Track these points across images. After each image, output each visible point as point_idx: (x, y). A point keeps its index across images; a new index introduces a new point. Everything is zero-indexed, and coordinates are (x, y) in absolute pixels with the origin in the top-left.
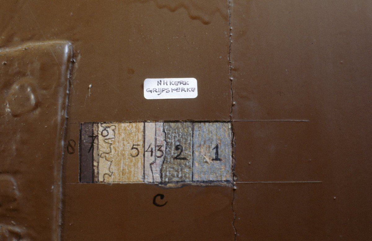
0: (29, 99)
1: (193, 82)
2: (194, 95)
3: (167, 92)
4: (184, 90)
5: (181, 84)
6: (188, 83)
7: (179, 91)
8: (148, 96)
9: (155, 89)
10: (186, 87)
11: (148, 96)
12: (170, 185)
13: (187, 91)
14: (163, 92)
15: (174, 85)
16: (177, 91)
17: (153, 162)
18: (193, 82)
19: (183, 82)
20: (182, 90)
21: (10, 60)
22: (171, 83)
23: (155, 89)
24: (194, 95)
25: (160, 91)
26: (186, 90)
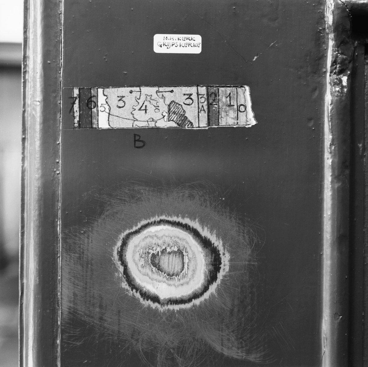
0: (158, 298)
1: (198, 39)
2: (198, 50)
3: (176, 46)
4: (188, 39)
5: (188, 40)
6: (194, 39)
7: (186, 47)
8: (157, 49)
9: (166, 44)
10: (192, 42)
11: (157, 49)
12: (31, 323)
13: (194, 47)
14: (172, 46)
15: (197, 47)
16: (200, 113)
17: (171, 304)
18: (198, 39)
19: (189, 38)
20: (187, 39)
21: (57, 5)
22: (180, 45)
23: (166, 44)
24: (198, 50)
25: (169, 45)
26: (190, 39)
